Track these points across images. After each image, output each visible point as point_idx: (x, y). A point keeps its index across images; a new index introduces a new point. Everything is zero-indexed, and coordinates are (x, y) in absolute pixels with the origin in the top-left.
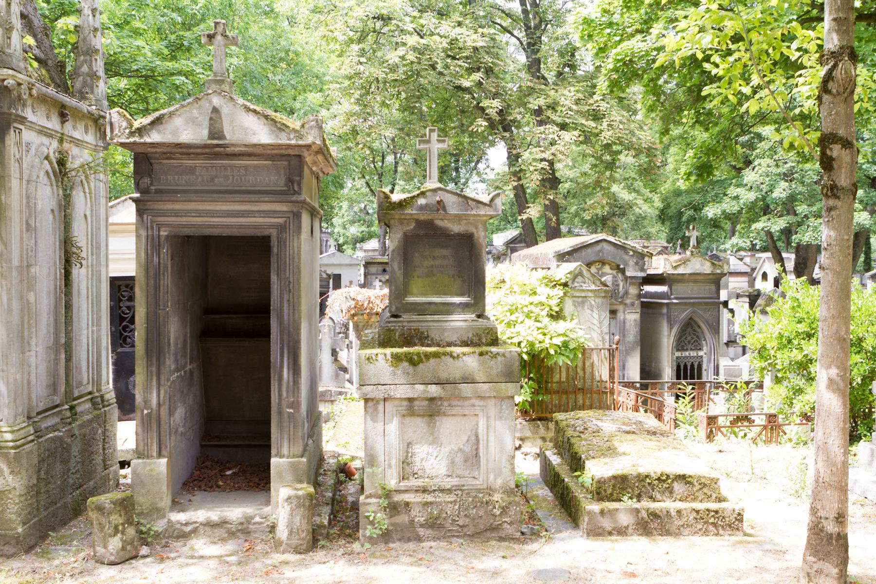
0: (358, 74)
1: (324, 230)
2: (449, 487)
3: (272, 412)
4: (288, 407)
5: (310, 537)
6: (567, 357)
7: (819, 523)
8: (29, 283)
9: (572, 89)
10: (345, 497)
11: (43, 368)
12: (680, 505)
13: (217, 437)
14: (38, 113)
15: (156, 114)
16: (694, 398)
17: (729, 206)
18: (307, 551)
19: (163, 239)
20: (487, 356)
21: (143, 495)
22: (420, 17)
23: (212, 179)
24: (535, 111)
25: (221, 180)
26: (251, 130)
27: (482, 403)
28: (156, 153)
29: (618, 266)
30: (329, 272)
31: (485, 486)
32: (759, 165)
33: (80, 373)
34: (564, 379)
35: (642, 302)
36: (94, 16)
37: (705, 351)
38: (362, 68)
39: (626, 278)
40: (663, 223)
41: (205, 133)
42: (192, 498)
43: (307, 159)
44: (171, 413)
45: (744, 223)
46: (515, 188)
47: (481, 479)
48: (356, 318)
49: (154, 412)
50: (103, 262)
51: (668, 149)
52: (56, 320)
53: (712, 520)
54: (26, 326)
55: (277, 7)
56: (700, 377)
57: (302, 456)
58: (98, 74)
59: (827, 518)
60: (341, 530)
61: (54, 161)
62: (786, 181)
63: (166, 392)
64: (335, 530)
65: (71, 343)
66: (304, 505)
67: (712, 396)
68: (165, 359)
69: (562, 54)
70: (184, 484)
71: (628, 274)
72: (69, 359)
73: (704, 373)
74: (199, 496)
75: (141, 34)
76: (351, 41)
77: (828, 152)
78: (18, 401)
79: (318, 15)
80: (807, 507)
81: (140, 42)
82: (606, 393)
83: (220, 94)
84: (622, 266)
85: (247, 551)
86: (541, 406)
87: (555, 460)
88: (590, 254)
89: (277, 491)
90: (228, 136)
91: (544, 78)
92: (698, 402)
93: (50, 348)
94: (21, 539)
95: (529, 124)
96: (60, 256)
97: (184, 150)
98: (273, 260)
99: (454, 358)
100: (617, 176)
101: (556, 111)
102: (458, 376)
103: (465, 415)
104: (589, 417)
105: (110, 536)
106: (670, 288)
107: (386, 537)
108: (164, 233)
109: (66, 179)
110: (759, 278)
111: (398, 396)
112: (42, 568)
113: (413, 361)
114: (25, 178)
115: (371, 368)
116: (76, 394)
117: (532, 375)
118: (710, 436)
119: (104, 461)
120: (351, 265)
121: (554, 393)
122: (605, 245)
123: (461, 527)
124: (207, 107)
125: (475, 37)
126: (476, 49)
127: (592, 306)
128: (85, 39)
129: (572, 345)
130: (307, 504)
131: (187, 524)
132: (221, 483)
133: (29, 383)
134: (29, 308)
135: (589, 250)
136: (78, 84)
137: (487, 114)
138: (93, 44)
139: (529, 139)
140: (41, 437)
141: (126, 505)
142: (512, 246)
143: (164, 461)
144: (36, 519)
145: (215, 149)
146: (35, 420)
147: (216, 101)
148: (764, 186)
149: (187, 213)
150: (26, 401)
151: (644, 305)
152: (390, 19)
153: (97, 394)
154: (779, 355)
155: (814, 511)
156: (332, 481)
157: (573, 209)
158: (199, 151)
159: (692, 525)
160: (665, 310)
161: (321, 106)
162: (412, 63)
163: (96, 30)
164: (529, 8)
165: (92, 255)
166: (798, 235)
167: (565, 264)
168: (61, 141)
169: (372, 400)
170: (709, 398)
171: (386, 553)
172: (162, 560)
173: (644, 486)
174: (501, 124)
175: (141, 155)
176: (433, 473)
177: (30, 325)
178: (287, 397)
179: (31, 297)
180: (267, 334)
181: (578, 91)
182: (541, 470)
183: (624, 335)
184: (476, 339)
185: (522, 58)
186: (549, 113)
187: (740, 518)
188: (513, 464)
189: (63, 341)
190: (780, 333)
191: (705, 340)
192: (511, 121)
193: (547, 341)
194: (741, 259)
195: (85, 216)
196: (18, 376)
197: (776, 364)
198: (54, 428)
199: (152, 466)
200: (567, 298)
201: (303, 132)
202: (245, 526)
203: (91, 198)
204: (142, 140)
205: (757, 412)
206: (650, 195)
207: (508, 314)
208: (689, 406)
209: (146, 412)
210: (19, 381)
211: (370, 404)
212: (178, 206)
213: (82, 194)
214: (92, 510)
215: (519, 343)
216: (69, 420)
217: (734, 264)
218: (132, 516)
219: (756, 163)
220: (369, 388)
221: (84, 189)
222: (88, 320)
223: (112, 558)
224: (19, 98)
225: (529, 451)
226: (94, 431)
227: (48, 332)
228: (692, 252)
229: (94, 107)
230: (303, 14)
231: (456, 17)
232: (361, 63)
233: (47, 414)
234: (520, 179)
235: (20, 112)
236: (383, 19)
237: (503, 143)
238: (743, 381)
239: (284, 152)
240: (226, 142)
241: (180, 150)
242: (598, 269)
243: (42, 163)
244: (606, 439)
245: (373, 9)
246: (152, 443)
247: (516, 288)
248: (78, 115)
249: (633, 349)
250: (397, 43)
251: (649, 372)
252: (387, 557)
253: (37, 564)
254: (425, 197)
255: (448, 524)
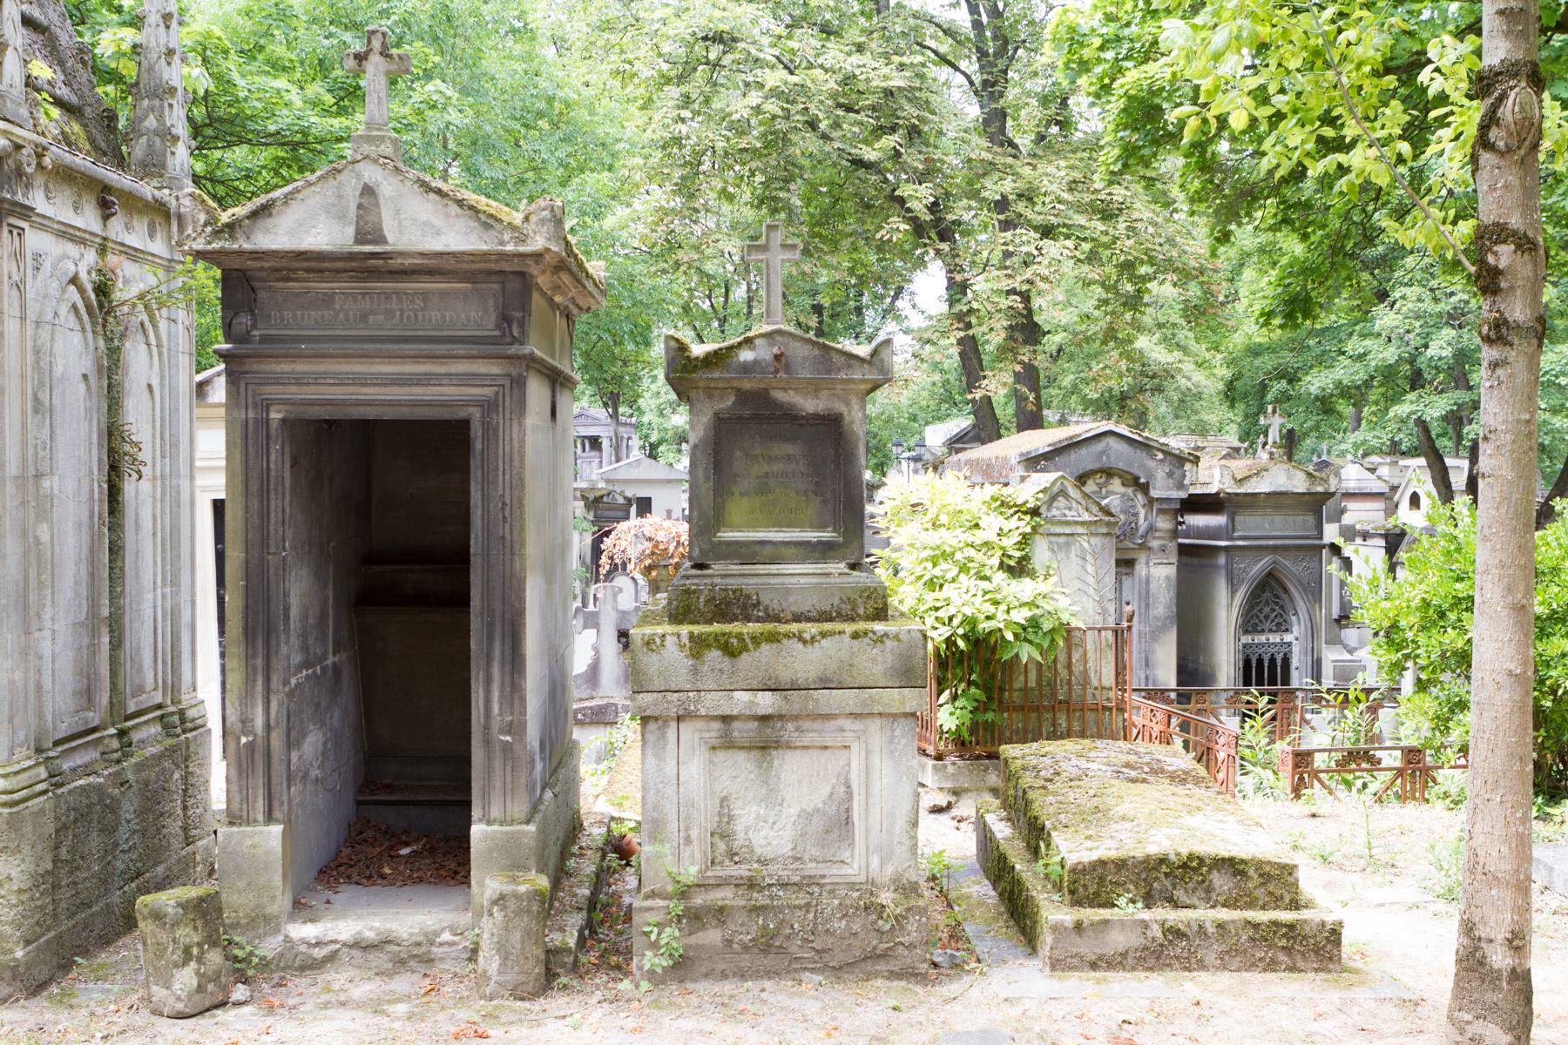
0: (678, 141)
1: (623, 419)
2: (796, 879)
3: (474, 742)
4: (502, 732)
5: (539, 970)
6: (1039, 646)
7: (1477, 949)
8: (44, 508)
9: (1063, 163)
10: (617, 896)
11: (66, 662)
12: (1224, 914)
13: (388, 786)
14: (57, 200)
15: (262, 199)
16: (1274, 719)
17: (1345, 372)
18: (534, 995)
19: (274, 425)
20: (867, 640)
21: (239, 892)
22: (790, 37)
23: (364, 317)
24: (997, 203)
25: (381, 318)
26: (421, 227)
27: (857, 725)
28: (262, 269)
29: (1137, 479)
30: (629, 494)
31: (862, 879)
32: (1403, 297)
33: (140, 670)
34: (1032, 683)
35: (1181, 546)
36: (168, 27)
37: (1296, 633)
38: (684, 129)
39: (1151, 501)
40: (1232, 406)
41: (350, 231)
42: (333, 897)
43: (540, 280)
44: (290, 744)
45: (1376, 403)
46: (960, 342)
47: (856, 866)
48: (654, 573)
49: (260, 741)
50: (184, 470)
51: (1240, 274)
52: (92, 575)
53: (1283, 942)
54: (33, 585)
55: (536, 19)
56: (1286, 680)
57: (528, 822)
58: (174, 131)
59: (1491, 941)
60: (602, 956)
61: (89, 288)
62: (1453, 327)
63: (280, 704)
64: (592, 957)
65: (121, 616)
66: (529, 912)
67: (1308, 716)
68: (278, 645)
69: (1045, 101)
70: (321, 871)
71: (1154, 493)
72: (116, 645)
73: (1294, 674)
74: (347, 893)
75: (284, 69)
76: (668, 81)
77: (1491, 259)
78: (17, 721)
79: (606, 35)
80: (1455, 924)
81: (281, 83)
82: (1110, 709)
83: (375, 161)
84: (1142, 480)
85: (426, 994)
86: (992, 732)
87: (1001, 830)
88: (1085, 459)
89: (481, 885)
90: (390, 238)
91: (1012, 144)
92: (1280, 725)
93: (81, 624)
94: (22, 970)
95: (986, 227)
96: (100, 459)
97: (312, 264)
98: (474, 464)
99: (805, 642)
100: (1147, 320)
101: (1034, 204)
102: (812, 675)
103: (826, 748)
104: (1062, 754)
105: (176, 966)
106: (1232, 520)
107: (682, 968)
108: (276, 415)
109: (111, 320)
110: (1405, 503)
111: (703, 712)
112: (56, 1023)
113: (731, 650)
114: (31, 316)
115: (652, 663)
116: (132, 708)
117: (974, 677)
118: (1297, 792)
119: (185, 829)
120: (669, 481)
121: (1015, 709)
122: (1112, 441)
123: (818, 952)
124: (350, 185)
125: (886, 70)
126: (888, 93)
127: (1083, 550)
128: (151, 69)
129: (1047, 625)
130: (535, 908)
131: (318, 944)
132: (387, 871)
133: (39, 687)
134: (39, 553)
135: (1084, 451)
136: (138, 149)
137: (909, 210)
138: (166, 77)
139: (985, 254)
140: (62, 785)
141: (206, 911)
142: (957, 443)
143: (277, 829)
144: (53, 933)
145: (369, 266)
146: (51, 754)
147: (371, 173)
148: (1411, 336)
149: (317, 379)
150: (33, 721)
151: (1184, 550)
152: (734, 40)
153: (172, 709)
154: (1422, 639)
155: (1468, 928)
156: (593, 868)
157: (1067, 381)
158: (339, 265)
159: (1245, 951)
160: (1222, 560)
161: (613, 198)
162: (774, 117)
163: (170, 52)
164: (985, 19)
165: (163, 457)
166: (1474, 426)
167: (1035, 476)
168: (102, 251)
169: (656, 719)
170: (1303, 719)
171: (679, 1000)
172: (271, 1009)
173: (1157, 878)
174: (936, 227)
175: (235, 274)
176: (768, 853)
177: (41, 584)
178: (501, 714)
179: (44, 533)
180: (465, 601)
181: (1072, 167)
182: (979, 849)
183: (1147, 605)
184: (846, 609)
185: (973, 110)
186: (1020, 207)
187: (1335, 935)
188: (914, 838)
189: (105, 612)
190: (1424, 600)
191: (1296, 614)
192: (953, 222)
193: (1001, 616)
194: (1372, 470)
195: (150, 386)
196: (18, 675)
197: (1418, 656)
198: (88, 770)
199: (256, 839)
200: (1038, 537)
201: (529, 228)
202: (423, 949)
203: (160, 354)
204: (236, 246)
205: (1388, 744)
206: (1208, 356)
207: (929, 565)
208: (1262, 733)
209: (244, 740)
210: (20, 684)
211: (652, 726)
212: (301, 367)
213: (143, 347)
214: (145, 919)
215: (951, 619)
216: (116, 755)
217: (1352, 475)
218: (217, 930)
219: (1397, 294)
220: (649, 697)
221: (147, 337)
222: (155, 574)
223: (180, 1006)
224: (19, 173)
225: (965, 815)
226: (166, 776)
227: (77, 595)
228: (1271, 453)
229: (166, 191)
230: (577, 30)
231: (853, 34)
232: (683, 120)
233: (73, 744)
234: (969, 326)
235: (19, 198)
236: (721, 41)
237: (939, 263)
238: (1360, 687)
239: (492, 266)
240: (388, 248)
241: (306, 264)
242: (1100, 486)
243: (64, 291)
244: (1092, 792)
245: (703, 22)
246: (255, 797)
247: (944, 519)
248: (134, 205)
249: (1163, 629)
250: (747, 84)
251: (1193, 672)
252: (680, 1007)
253: (49, 1016)
254: (753, 349)
255: (794, 947)
